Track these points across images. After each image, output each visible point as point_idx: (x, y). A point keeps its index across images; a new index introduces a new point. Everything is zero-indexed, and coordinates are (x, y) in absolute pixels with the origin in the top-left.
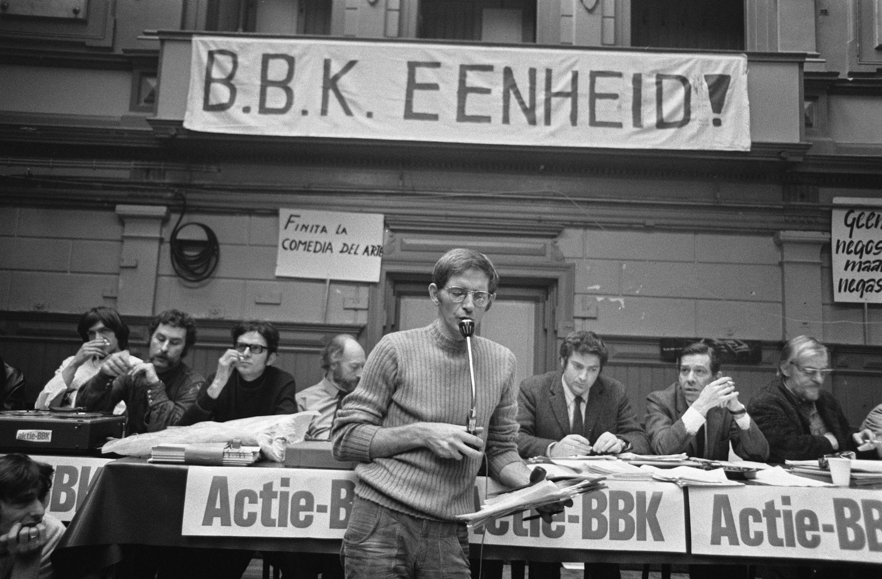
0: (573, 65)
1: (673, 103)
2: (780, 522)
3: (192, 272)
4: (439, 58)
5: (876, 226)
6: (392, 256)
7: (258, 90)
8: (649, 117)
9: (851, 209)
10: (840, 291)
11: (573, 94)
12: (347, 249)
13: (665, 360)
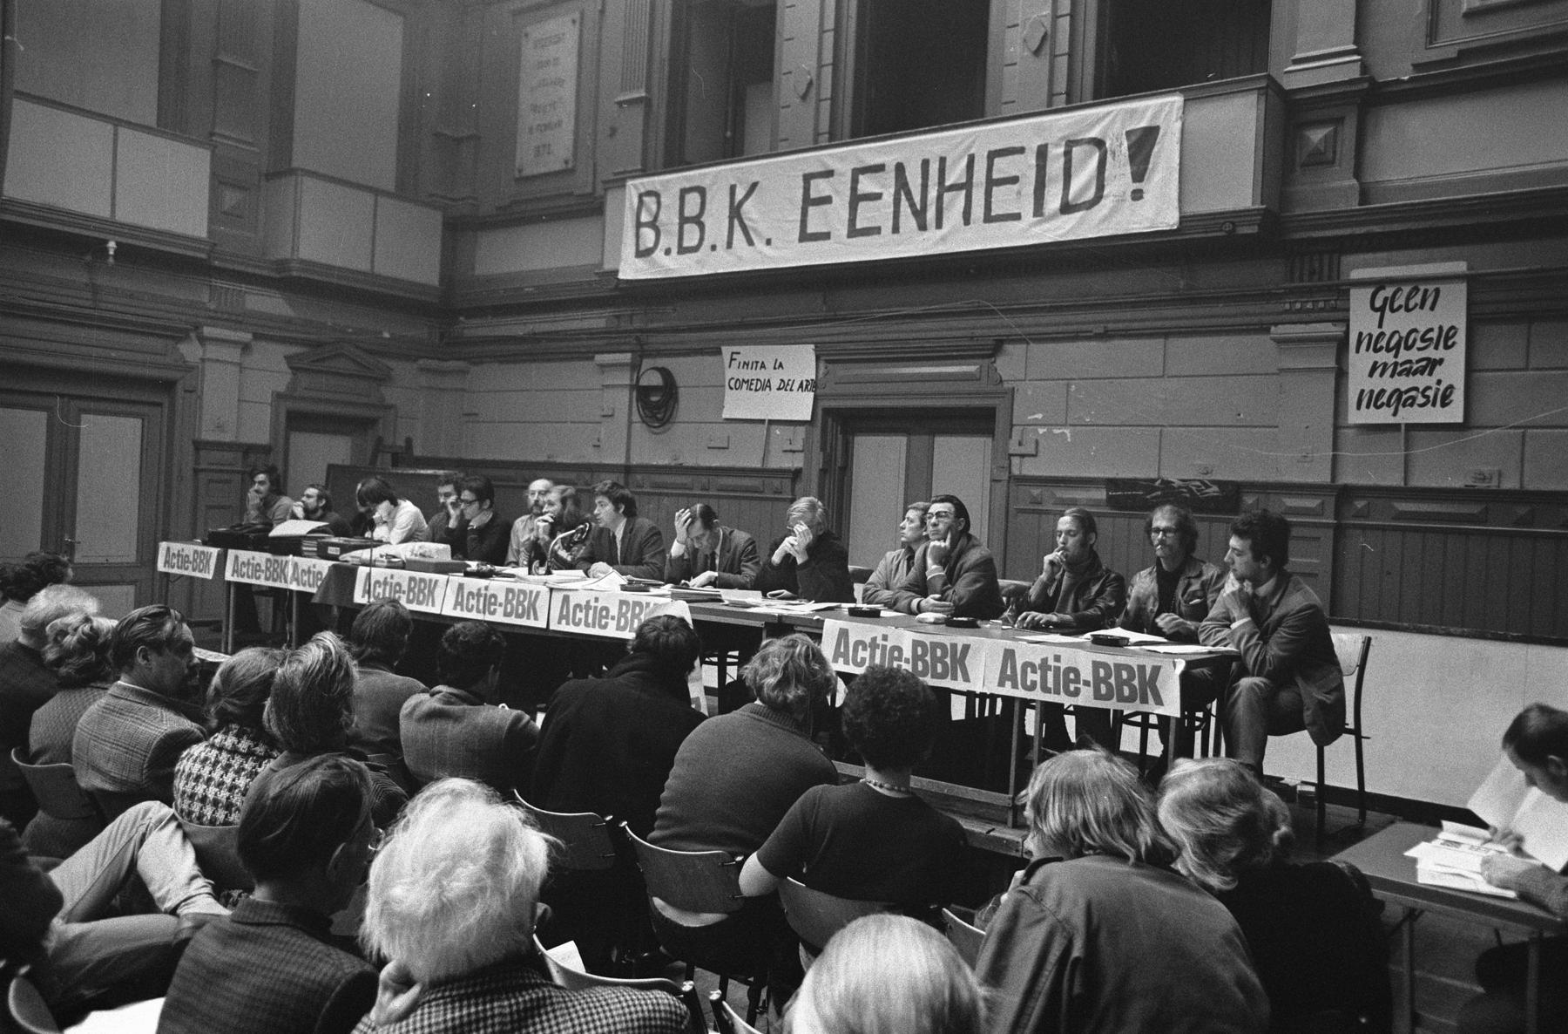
0: (970, 147)
1: (1084, 176)
2: (1050, 675)
3: (654, 417)
4: (833, 165)
5: (1422, 307)
6: (827, 391)
7: (676, 228)
8: (1053, 202)
9: (1380, 284)
10: (1359, 407)
11: (967, 186)
12: (784, 386)
13: (1113, 507)
